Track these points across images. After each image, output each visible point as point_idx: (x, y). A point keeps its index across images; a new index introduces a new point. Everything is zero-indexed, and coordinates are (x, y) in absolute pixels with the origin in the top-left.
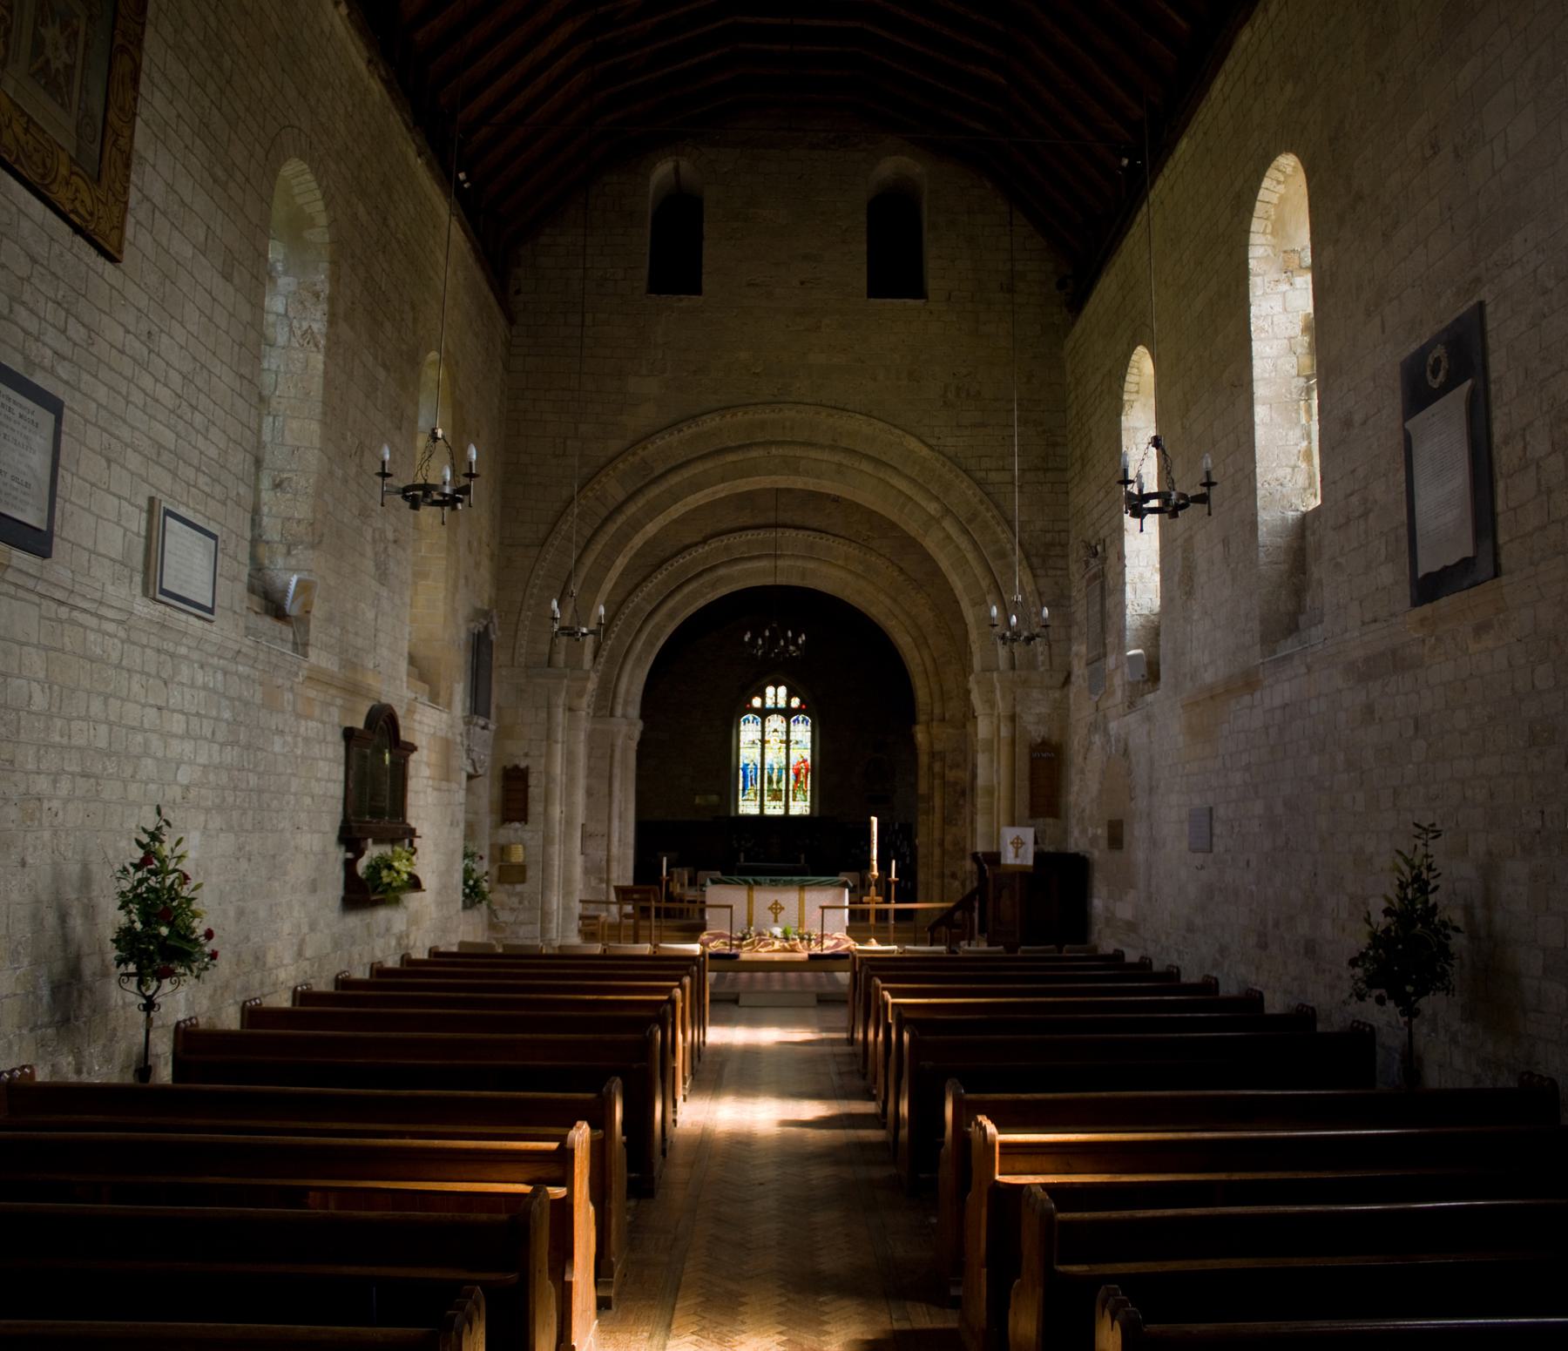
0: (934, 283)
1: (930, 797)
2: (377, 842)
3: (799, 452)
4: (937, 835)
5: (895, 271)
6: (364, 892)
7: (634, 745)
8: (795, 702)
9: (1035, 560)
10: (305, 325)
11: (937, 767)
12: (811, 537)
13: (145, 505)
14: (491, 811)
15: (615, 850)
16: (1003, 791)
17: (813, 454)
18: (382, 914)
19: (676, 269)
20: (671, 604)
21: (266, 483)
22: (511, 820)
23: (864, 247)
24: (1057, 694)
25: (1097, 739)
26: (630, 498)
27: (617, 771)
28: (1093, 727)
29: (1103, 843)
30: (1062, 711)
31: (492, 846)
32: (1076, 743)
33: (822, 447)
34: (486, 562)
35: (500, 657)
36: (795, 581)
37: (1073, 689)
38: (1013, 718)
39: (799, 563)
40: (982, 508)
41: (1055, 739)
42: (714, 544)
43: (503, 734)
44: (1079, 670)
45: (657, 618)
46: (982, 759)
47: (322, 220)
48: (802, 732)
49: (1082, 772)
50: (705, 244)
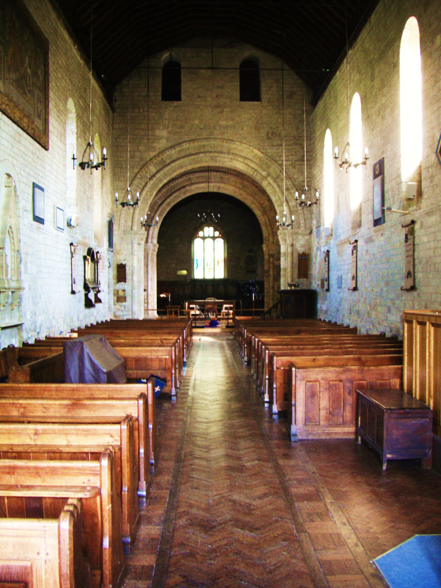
0: (264, 96)
1: (268, 271)
4: (271, 285)
7: (155, 253)
10: (70, 142)
11: (271, 260)
12: (222, 175)
13: (52, 206)
14: (114, 279)
16: (289, 270)
19: (172, 93)
20: (168, 200)
22: (120, 281)
23: (239, 83)
24: (307, 237)
26: (158, 172)
27: (150, 263)
29: (320, 287)
31: (114, 290)
32: (313, 255)
35: (115, 227)
36: (215, 190)
37: (313, 235)
38: (292, 245)
41: (307, 252)
42: (184, 178)
44: (314, 230)
45: (163, 205)
46: (282, 259)
47: (74, 111)
48: (220, 243)
49: (315, 263)
50: (182, 83)
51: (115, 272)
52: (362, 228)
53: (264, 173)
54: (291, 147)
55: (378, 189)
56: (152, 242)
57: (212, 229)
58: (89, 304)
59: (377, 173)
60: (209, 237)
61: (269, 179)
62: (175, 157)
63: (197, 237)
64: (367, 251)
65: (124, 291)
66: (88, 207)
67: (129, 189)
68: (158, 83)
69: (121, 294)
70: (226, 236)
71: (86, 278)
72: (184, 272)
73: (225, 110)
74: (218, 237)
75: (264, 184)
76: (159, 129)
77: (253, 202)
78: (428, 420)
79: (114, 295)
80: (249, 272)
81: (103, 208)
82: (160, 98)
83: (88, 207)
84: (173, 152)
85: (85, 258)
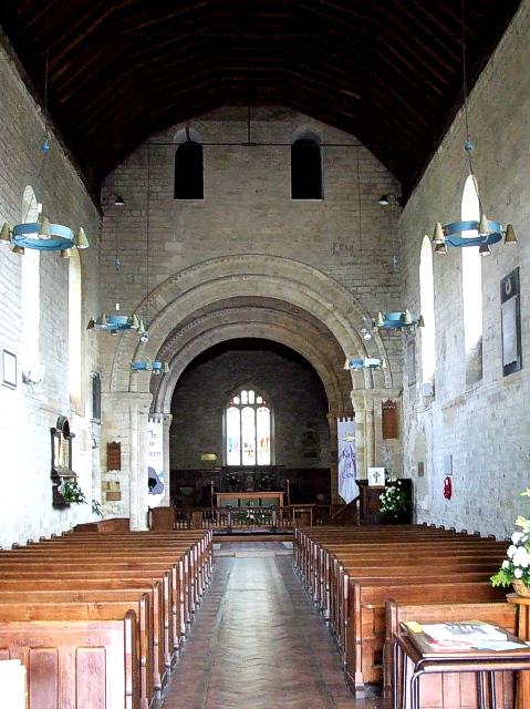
3: (256, 278)
5: (307, 182)
6: (61, 502)
12: (267, 311)
19: (189, 184)
28: (412, 417)
29: (417, 473)
33: (268, 276)
34: (96, 341)
35: (104, 388)
39: (259, 326)
40: (354, 306)
42: (211, 316)
44: (406, 388)
48: (265, 415)
51: (105, 454)
52: (483, 380)
53: (329, 306)
54: (369, 266)
55: (509, 317)
56: (162, 412)
57: (252, 393)
59: (508, 292)
60: (248, 405)
61: (336, 314)
62: (195, 283)
63: (231, 406)
64: (493, 414)
65: (118, 483)
66: (59, 354)
69: (113, 488)
70: (273, 404)
71: (56, 465)
72: (212, 457)
73: (270, 211)
74: (262, 405)
75: (329, 322)
76: (170, 241)
77: (312, 352)
78: (280, 495)
79: (103, 489)
80: (308, 455)
81: (83, 357)
82: (172, 194)
83: (59, 354)
84: (191, 274)
85: (53, 431)
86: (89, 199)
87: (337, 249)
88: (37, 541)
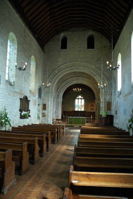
2: (24, 111)
3: (79, 67)
4: (98, 113)
5: (91, 44)
8: (82, 98)
9: (108, 80)
12: (83, 78)
15: (59, 114)
16: (103, 107)
17: (80, 67)
18: (26, 119)
19: (64, 46)
20: (66, 86)
21: (10, 70)
22: (46, 109)
25: (115, 101)
27: (59, 105)
28: (114, 100)
29: (115, 114)
30: (111, 98)
32: (112, 102)
35: (42, 91)
38: (105, 99)
43: (43, 100)
44: (113, 93)
46: (101, 104)
47: (16, 40)
48: (83, 101)
51: (42, 107)
57: (81, 96)
58: (22, 117)
60: (80, 99)
61: (97, 75)
67: (23, 62)
68: (60, 43)
86: (40, 47)
87: (97, 60)
88: (22, 126)
